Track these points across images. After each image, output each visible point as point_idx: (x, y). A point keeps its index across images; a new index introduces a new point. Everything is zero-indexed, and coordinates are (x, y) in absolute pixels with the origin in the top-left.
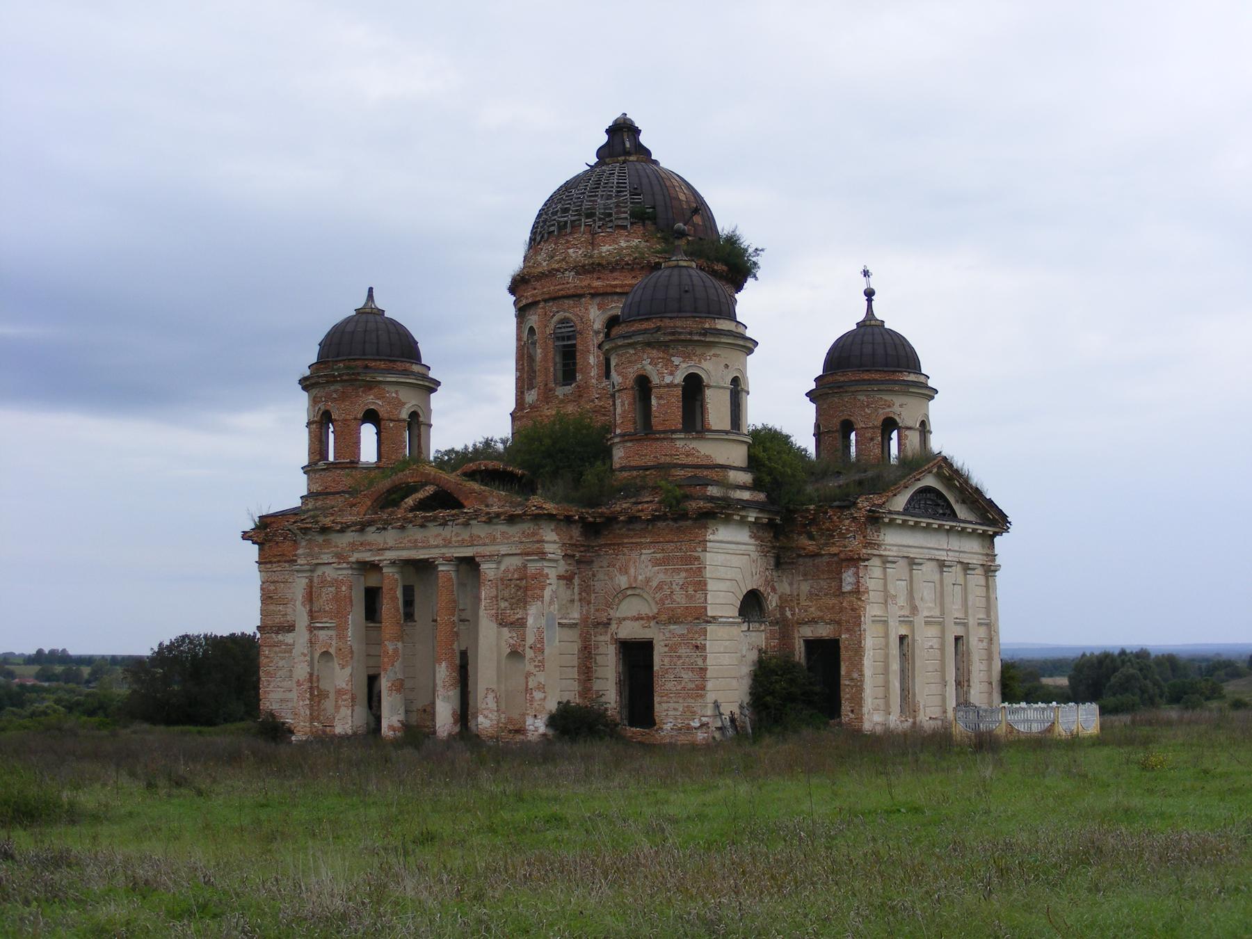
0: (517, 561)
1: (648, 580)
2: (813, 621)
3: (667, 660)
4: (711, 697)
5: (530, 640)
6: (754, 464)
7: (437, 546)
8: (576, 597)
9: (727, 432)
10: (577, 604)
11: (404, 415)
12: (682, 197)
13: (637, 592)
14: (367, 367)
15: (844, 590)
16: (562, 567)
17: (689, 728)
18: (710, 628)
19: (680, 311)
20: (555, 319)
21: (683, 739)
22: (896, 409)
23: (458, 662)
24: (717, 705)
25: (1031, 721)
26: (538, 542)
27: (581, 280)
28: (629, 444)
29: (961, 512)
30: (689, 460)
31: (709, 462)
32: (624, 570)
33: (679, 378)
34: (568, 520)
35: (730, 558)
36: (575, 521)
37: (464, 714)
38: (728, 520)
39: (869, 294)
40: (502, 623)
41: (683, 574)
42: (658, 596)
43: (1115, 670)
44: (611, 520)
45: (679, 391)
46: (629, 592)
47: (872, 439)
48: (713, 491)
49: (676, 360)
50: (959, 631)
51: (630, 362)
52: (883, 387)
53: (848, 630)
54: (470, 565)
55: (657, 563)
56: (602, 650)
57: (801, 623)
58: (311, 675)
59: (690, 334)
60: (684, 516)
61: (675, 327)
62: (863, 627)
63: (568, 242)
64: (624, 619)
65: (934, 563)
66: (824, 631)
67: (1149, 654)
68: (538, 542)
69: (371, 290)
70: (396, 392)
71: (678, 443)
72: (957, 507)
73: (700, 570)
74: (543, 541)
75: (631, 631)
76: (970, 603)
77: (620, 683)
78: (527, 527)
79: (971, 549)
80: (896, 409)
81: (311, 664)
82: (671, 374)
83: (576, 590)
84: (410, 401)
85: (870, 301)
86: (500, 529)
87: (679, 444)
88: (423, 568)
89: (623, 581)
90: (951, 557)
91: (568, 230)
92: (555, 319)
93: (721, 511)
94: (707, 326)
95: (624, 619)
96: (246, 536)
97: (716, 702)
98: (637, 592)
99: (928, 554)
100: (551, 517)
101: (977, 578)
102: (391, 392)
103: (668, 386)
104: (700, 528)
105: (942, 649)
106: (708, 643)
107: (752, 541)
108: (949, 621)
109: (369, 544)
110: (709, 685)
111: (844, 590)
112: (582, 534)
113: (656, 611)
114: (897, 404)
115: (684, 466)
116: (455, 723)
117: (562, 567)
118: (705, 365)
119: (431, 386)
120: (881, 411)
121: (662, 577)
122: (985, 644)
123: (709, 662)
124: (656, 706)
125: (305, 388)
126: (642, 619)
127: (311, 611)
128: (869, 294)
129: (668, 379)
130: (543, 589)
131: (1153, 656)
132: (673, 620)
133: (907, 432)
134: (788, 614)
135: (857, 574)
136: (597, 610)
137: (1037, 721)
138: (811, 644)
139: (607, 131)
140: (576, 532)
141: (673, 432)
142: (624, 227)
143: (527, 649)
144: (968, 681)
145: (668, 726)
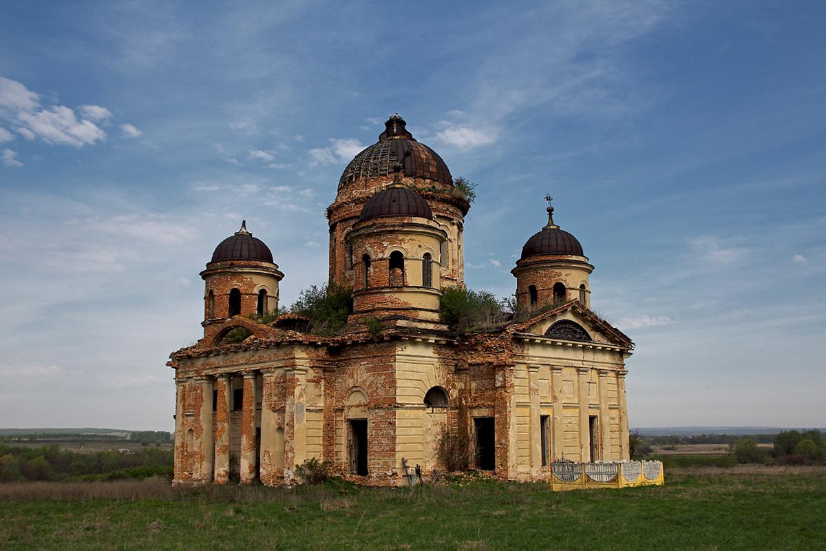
0: (281, 371)
1: (365, 381)
2: (478, 407)
3: (374, 432)
4: (399, 456)
5: (287, 420)
6: (442, 308)
7: (242, 364)
8: (323, 393)
9: (418, 287)
10: (322, 397)
11: (256, 291)
12: (423, 156)
13: (358, 389)
14: (232, 264)
15: (496, 386)
16: (311, 374)
17: (386, 475)
18: (397, 411)
19: (389, 214)
20: (345, 232)
21: (382, 483)
22: (563, 277)
23: (81, 434)
24: (404, 462)
25: (602, 474)
26: (292, 358)
27: (358, 208)
28: (359, 298)
29: (596, 337)
30: (393, 306)
31: (407, 306)
32: (352, 376)
33: (387, 255)
34: (313, 345)
35: (417, 368)
36: (319, 346)
37: (256, 468)
38: (413, 342)
39: (550, 211)
40: (274, 411)
41: (383, 377)
42: (369, 391)
43: (799, 440)
44: (343, 345)
45: (387, 263)
46: (354, 389)
47: (548, 296)
48: (400, 323)
49: (385, 244)
50: (593, 412)
51: (359, 247)
52: (554, 264)
53: (499, 412)
54: (257, 374)
55: (368, 370)
56: (339, 426)
57: (472, 408)
58: (183, 443)
59: (394, 226)
60: (381, 340)
61: (383, 226)
62: (508, 409)
63: (353, 186)
64: (352, 406)
65: (574, 369)
66: (484, 413)
67: (819, 432)
68: (292, 358)
69: (244, 222)
70: (251, 278)
71: (386, 295)
72: (591, 334)
73: (393, 374)
74: (294, 358)
75: (355, 414)
76: (602, 395)
77: (350, 447)
78: (288, 350)
79: (605, 361)
80: (563, 277)
81: (183, 437)
82: (382, 252)
83: (323, 388)
84: (260, 283)
85: (550, 215)
86: (272, 353)
87: (387, 295)
88: (235, 377)
89: (350, 382)
90: (586, 365)
91: (354, 180)
92: (345, 232)
93: (411, 337)
94: (406, 221)
95: (352, 406)
96: (168, 364)
97: (403, 459)
98: (358, 389)
99: (565, 363)
100: (300, 343)
101: (611, 378)
102: (248, 278)
103: (380, 259)
104: (391, 347)
105: (580, 424)
106: (397, 421)
107: (436, 355)
108: (584, 406)
109: (211, 364)
110: (398, 448)
111: (496, 386)
112: (326, 354)
113: (368, 401)
114: (564, 275)
115: (388, 309)
116: (251, 472)
117: (311, 374)
118: (404, 245)
119: (278, 277)
120: (553, 279)
121: (371, 378)
122: (617, 421)
123: (397, 433)
124: (368, 461)
125: (204, 278)
126: (361, 406)
127: (184, 405)
128: (550, 211)
129: (380, 256)
130: (294, 388)
131: (800, 432)
132: (377, 407)
133: (571, 291)
134: (464, 402)
135: (504, 375)
136: (337, 401)
137: (606, 474)
138: (478, 421)
139: (386, 124)
140: (322, 353)
141: (383, 288)
142: (385, 175)
143: (286, 426)
144: (602, 445)
145: (244, 479)
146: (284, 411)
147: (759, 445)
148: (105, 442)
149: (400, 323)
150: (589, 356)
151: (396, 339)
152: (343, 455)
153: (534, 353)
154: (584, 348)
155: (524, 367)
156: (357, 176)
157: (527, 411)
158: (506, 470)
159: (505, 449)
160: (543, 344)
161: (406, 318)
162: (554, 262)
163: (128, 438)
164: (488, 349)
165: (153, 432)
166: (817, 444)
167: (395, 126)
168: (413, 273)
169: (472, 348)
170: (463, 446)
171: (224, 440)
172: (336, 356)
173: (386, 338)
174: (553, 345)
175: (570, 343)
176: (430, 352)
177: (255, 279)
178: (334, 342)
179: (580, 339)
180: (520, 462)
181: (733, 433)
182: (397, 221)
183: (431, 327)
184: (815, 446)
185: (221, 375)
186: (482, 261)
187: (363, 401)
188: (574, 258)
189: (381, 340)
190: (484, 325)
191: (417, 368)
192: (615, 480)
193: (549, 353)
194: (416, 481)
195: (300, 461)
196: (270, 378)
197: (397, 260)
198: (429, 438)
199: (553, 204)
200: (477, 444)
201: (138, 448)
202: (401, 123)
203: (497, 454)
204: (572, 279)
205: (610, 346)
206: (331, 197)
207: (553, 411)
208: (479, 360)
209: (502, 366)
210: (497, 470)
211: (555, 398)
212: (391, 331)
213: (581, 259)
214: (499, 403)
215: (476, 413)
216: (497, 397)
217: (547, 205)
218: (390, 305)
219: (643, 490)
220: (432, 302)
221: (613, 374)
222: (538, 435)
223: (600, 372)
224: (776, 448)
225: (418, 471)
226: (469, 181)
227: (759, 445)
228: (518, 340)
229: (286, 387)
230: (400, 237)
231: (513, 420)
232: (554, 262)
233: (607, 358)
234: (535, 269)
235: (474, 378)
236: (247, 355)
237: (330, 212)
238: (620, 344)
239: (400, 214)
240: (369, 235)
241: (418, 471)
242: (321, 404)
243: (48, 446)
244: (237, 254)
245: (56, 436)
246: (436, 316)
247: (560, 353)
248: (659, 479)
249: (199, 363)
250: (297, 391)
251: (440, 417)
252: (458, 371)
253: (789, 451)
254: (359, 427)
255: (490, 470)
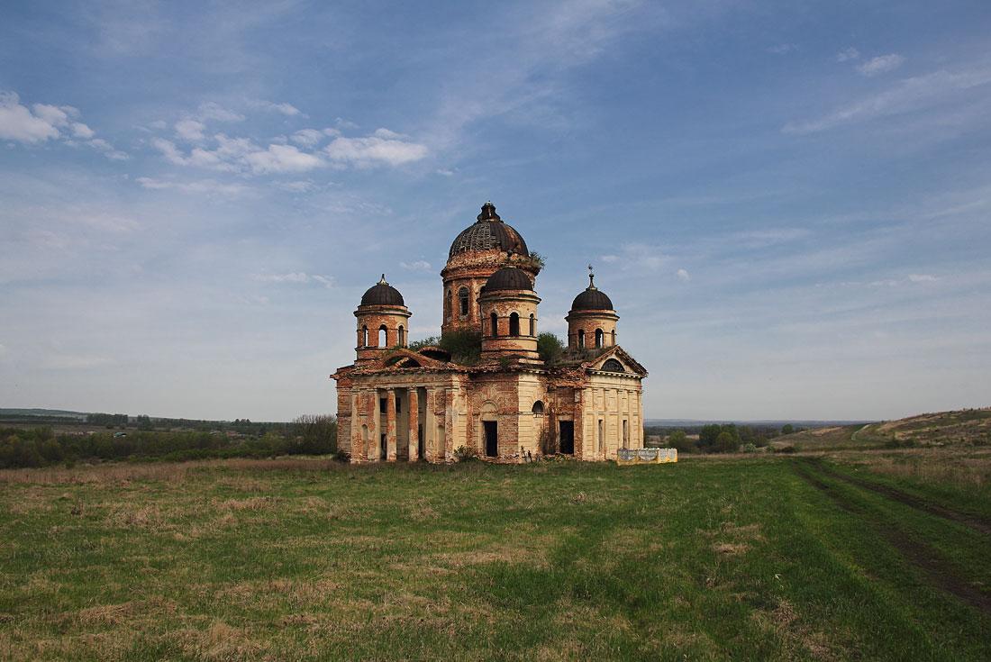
0: (441, 389)
2: (563, 414)
4: (520, 445)
11: (397, 327)
12: (512, 237)
29: (627, 368)
33: (509, 315)
34: (463, 373)
35: (529, 389)
37: (421, 450)
38: (528, 373)
39: (591, 276)
44: (480, 372)
48: (521, 361)
49: (507, 307)
50: (625, 418)
66: (567, 418)
72: (625, 367)
75: (488, 417)
84: (399, 321)
85: (591, 279)
89: (485, 397)
90: (622, 387)
93: (525, 370)
100: (456, 372)
102: (391, 317)
110: (519, 440)
115: (510, 350)
118: (519, 309)
119: (407, 315)
128: (591, 276)
129: (504, 315)
138: (562, 423)
140: (466, 377)
146: (444, 415)
147: (688, 437)
148: (66, 424)
149: (521, 361)
150: (624, 382)
151: (519, 371)
152: (480, 443)
153: (595, 380)
154: (622, 377)
155: (590, 389)
156: (468, 248)
157: (591, 417)
158: (581, 454)
159: (581, 440)
160: (601, 375)
161: (525, 358)
162: (597, 314)
163: (85, 421)
164: (569, 377)
165: (199, 421)
166: (733, 435)
167: (488, 211)
168: (524, 328)
169: (559, 376)
170: (553, 439)
171: (393, 433)
172: (476, 379)
173: (509, 370)
174: (606, 376)
175: (615, 374)
176: (535, 379)
177: (397, 318)
178: (474, 370)
179: (618, 371)
180: (589, 450)
181: (660, 425)
182: (512, 292)
183: (536, 362)
184: (731, 438)
185: (391, 389)
186: (547, 315)
187: (494, 409)
188: (609, 312)
189: (509, 371)
190: (567, 362)
191: (529, 389)
192: (656, 459)
193: (603, 380)
194: (529, 460)
195: (456, 447)
196: (433, 393)
197: (514, 319)
198: (535, 433)
199: (593, 272)
200: (563, 437)
201: (131, 432)
202: (493, 209)
203: (575, 444)
204: (606, 326)
205: (635, 375)
206: (444, 265)
207: (610, 419)
208: (564, 384)
209: (580, 389)
210: (575, 454)
211: (606, 409)
212: (516, 366)
213: (612, 312)
214: (577, 413)
215: (561, 418)
216: (575, 408)
217: (589, 272)
218: (510, 348)
219: (669, 465)
220: (533, 346)
221: (635, 393)
222: (597, 433)
223: (629, 392)
224: (701, 439)
225: (529, 454)
226: (541, 254)
227: (688, 437)
228: (589, 373)
229: (445, 400)
230: (517, 303)
231: (585, 423)
232: (597, 314)
233: (633, 383)
234: (583, 319)
235: (560, 396)
236: (413, 377)
237: (444, 273)
238: (640, 371)
239: (516, 288)
240: (497, 301)
241: (529, 454)
242: (465, 411)
243: (40, 427)
244: (383, 300)
245: (14, 416)
246: (537, 355)
247: (608, 380)
248: (675, 460)
249: (371, 380)
250: (454, 402)
251: (541, 420)
252: (549, 391)
253: (711, 442)
254: (491, 428)
255: (570, 453)
